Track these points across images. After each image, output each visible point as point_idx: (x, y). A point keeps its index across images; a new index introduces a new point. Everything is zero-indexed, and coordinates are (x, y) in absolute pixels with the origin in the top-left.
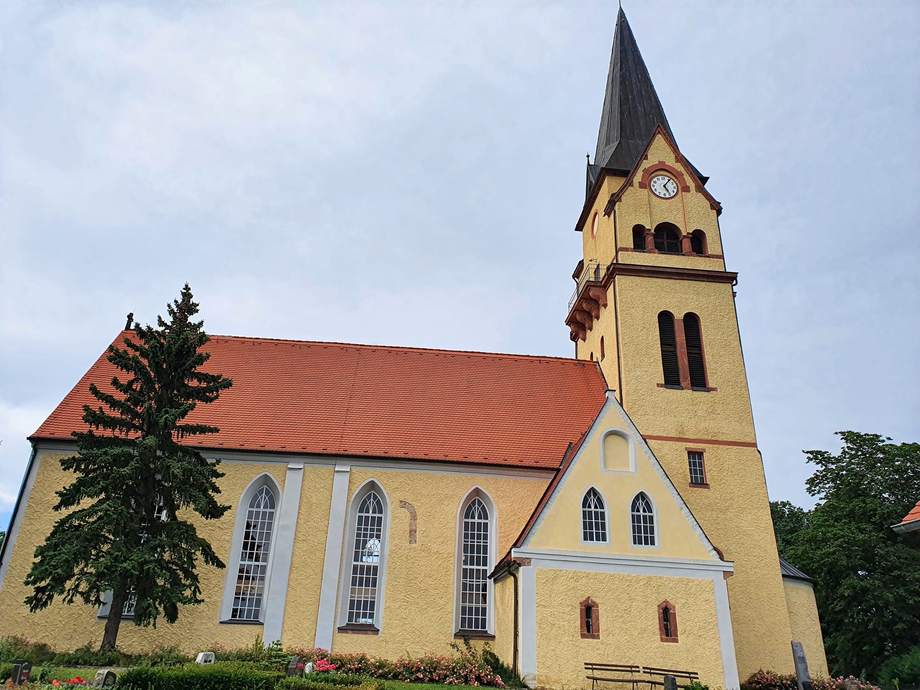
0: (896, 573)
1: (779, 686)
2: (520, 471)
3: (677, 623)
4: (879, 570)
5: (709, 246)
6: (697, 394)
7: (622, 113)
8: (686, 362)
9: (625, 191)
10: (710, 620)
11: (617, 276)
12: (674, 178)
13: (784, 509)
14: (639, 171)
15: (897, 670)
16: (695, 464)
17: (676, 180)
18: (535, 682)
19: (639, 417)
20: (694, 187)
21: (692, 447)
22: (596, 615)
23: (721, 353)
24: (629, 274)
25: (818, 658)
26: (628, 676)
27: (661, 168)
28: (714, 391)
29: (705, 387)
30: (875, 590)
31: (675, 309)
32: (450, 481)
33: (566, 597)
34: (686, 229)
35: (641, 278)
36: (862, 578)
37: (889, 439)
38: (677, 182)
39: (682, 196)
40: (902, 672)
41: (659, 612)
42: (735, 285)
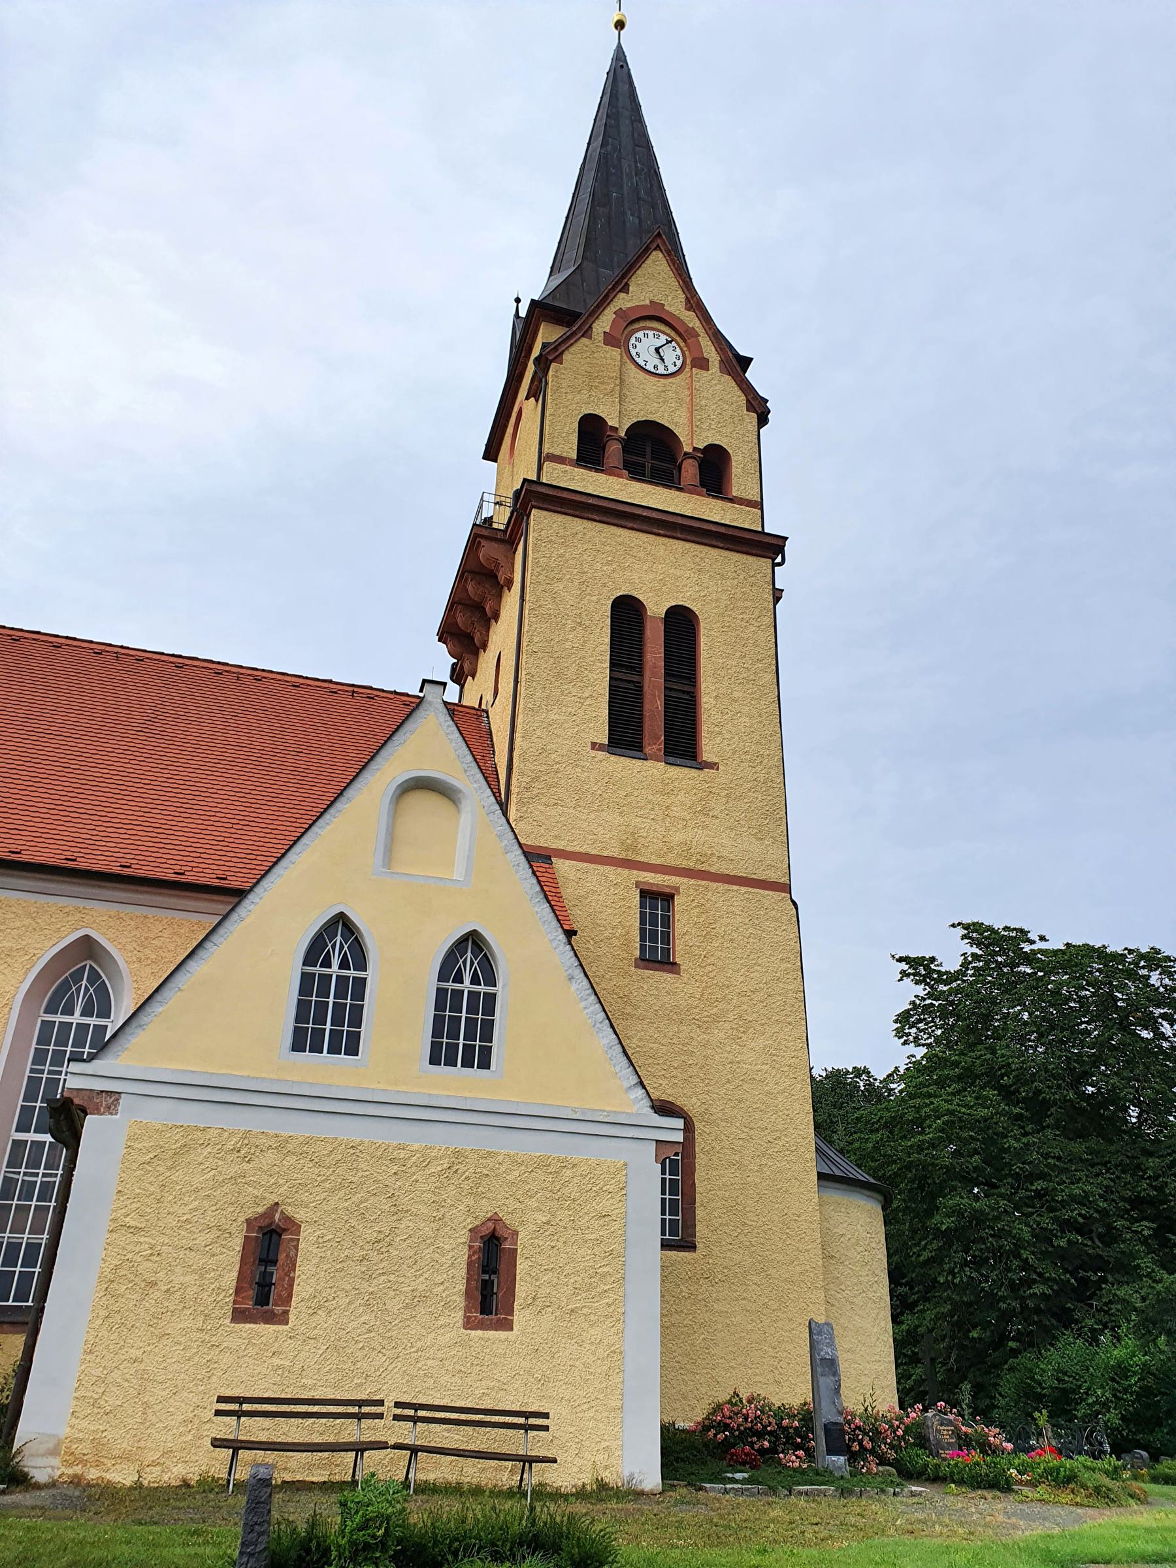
0: (1038, 1185)
1: (770, 1433)
2: (213, 901)
3: (518, 1278)
4: (1010, 1180)
5: (734, 480)
6: (674, 772)
7: (593, 218)
8: (660, 704)
9: (572, 344)
10: (606, 1269)
11: (533, 510)
12: (678, 339)
13: (858, 1080)
14: (607, 311)
15: (1032, 1379)
16: (654, 917)
17: (682, 344)
18: (56, 1461)
19: (541, 808)
20: (717, 364)
21: (651, 881)
22: (288, 1256)
23: (736, 694)
24: (559, 509)
25: (877, 1357)
26: (350, 1431)
27: (654, 316)
28: (713, 769)
29: (696, 760)
30: (997, 1218)
31: (651, 594)
32: (13, 916)
33: (206, 1204)
34: (692, 438)
35: (585, 521)
36: (977, 1198)
37: (1042, 938)
38: (685, 349)
39: (691, 376)
40: (1040, 1384)
41: (470, 1247)
42: (779, 565)
